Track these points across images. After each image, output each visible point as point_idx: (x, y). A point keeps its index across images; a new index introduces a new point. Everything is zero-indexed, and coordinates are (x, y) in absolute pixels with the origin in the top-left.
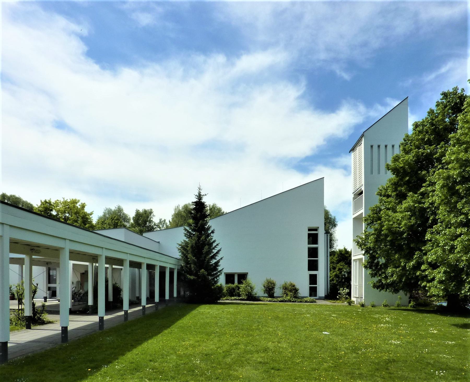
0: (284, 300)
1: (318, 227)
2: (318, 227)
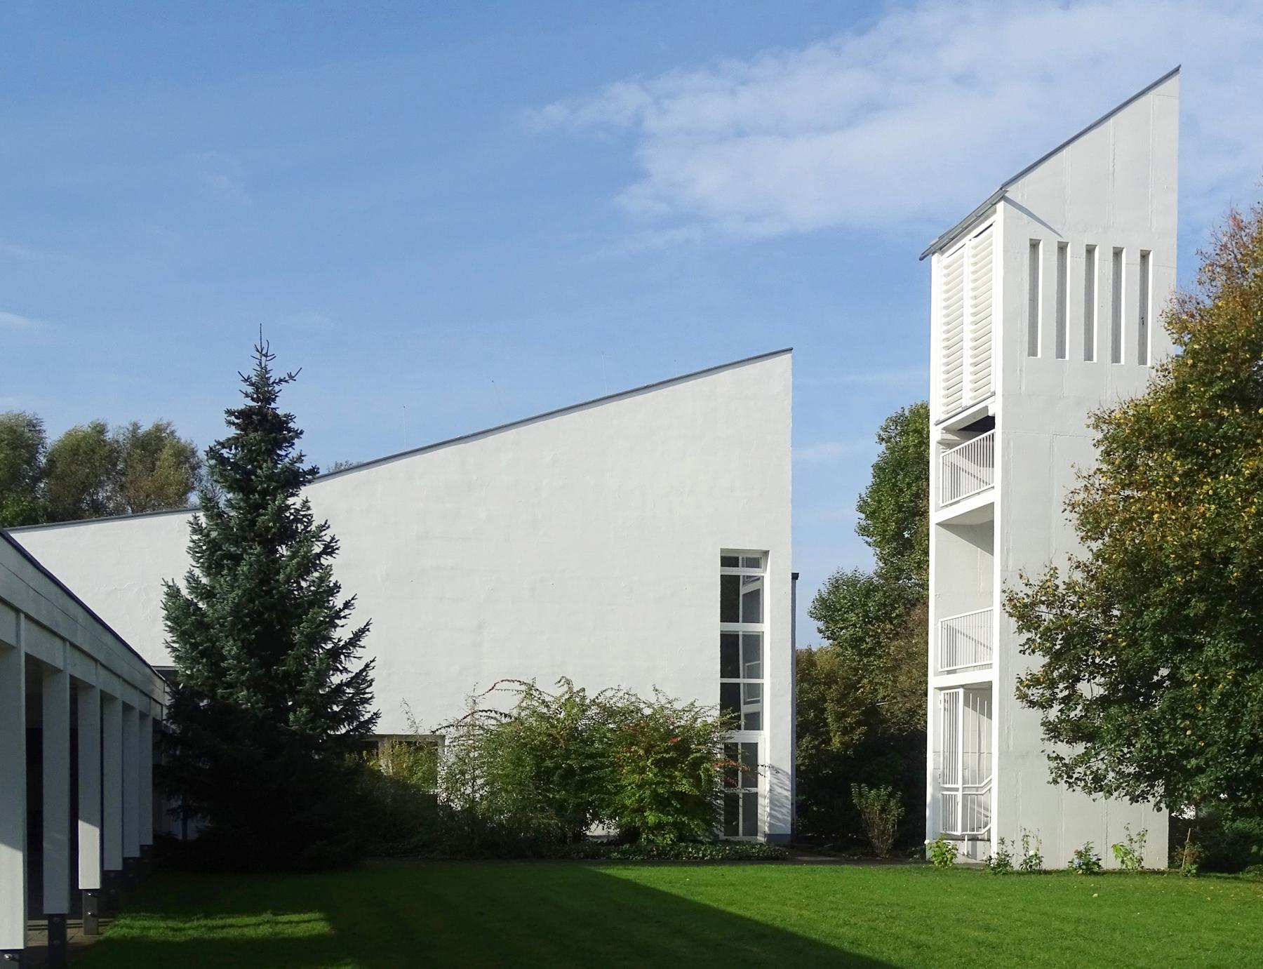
1: (766, 553)
2: (766, 553)
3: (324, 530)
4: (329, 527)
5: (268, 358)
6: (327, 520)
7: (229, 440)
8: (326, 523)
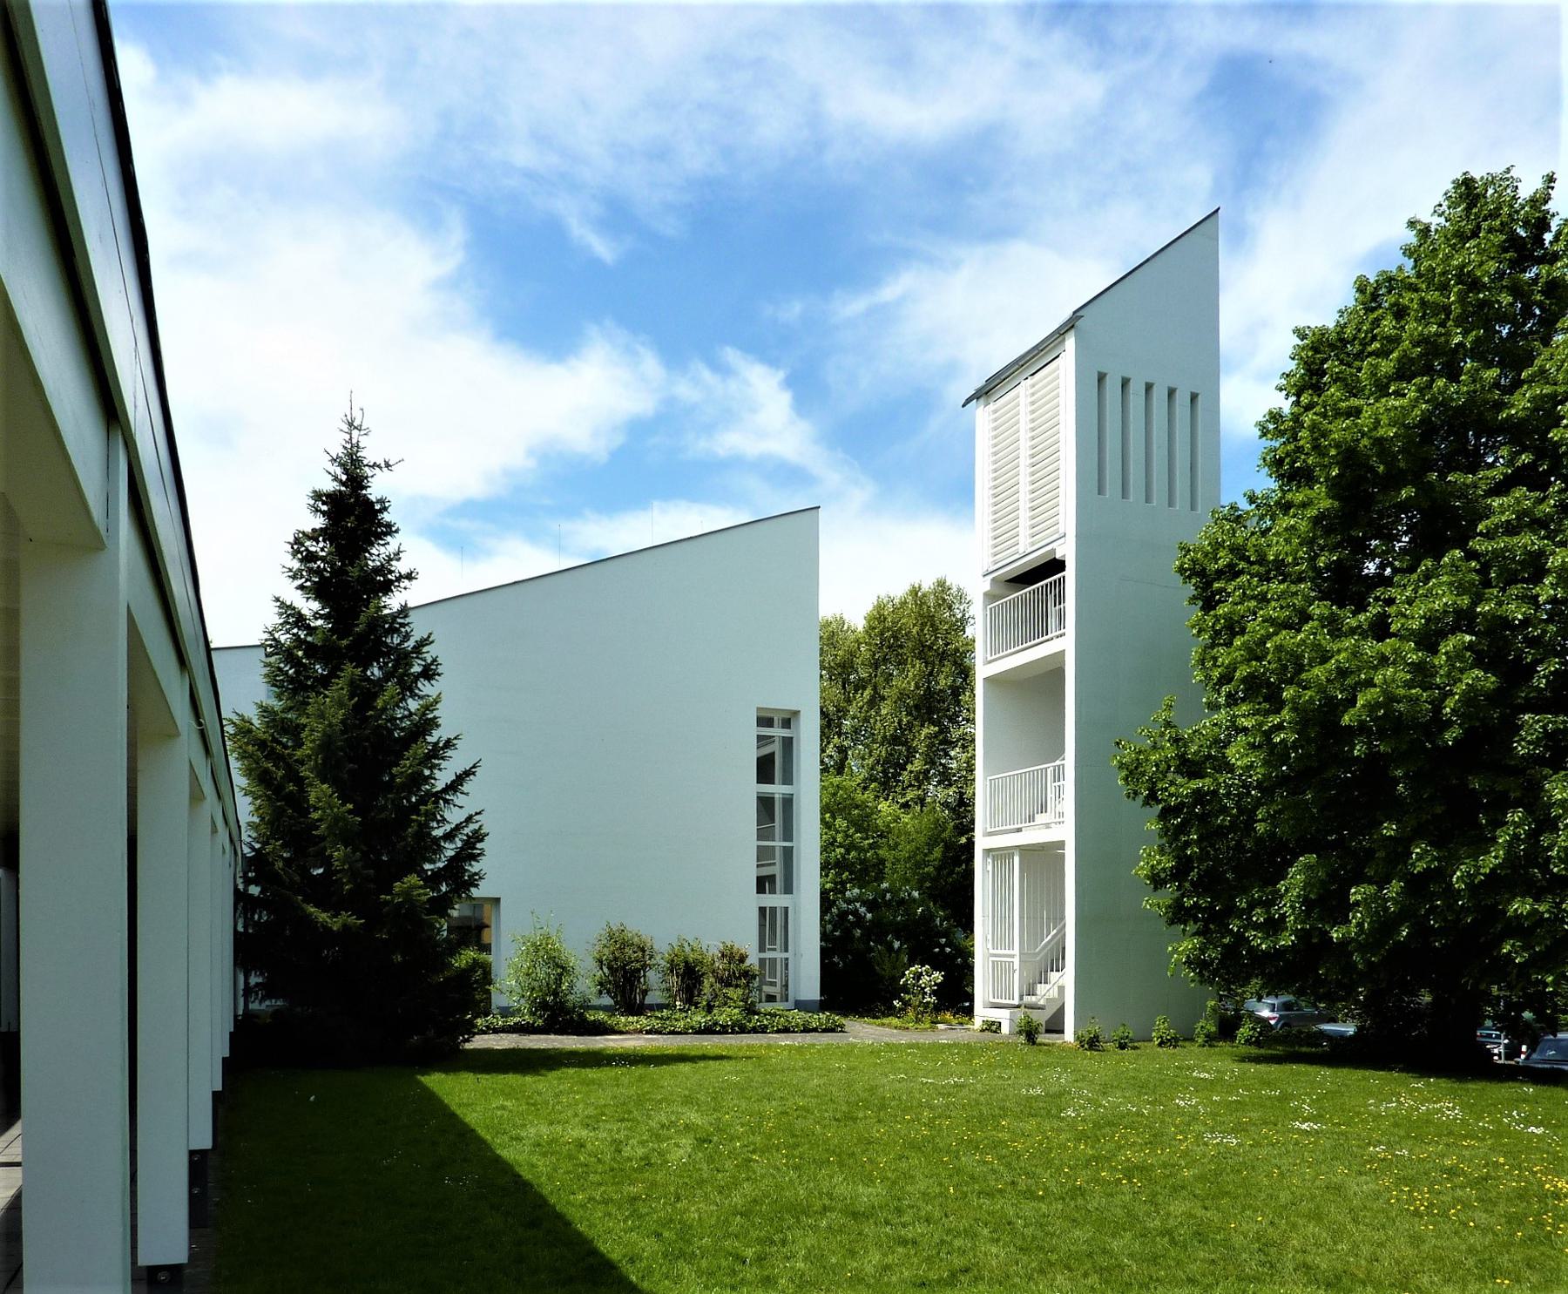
0: (716, 1024)
3: (427, 644)
4: (432, 642)
5: (362, 432)
6: (431, 634)
7: (314, 530)
8: (429, 637)
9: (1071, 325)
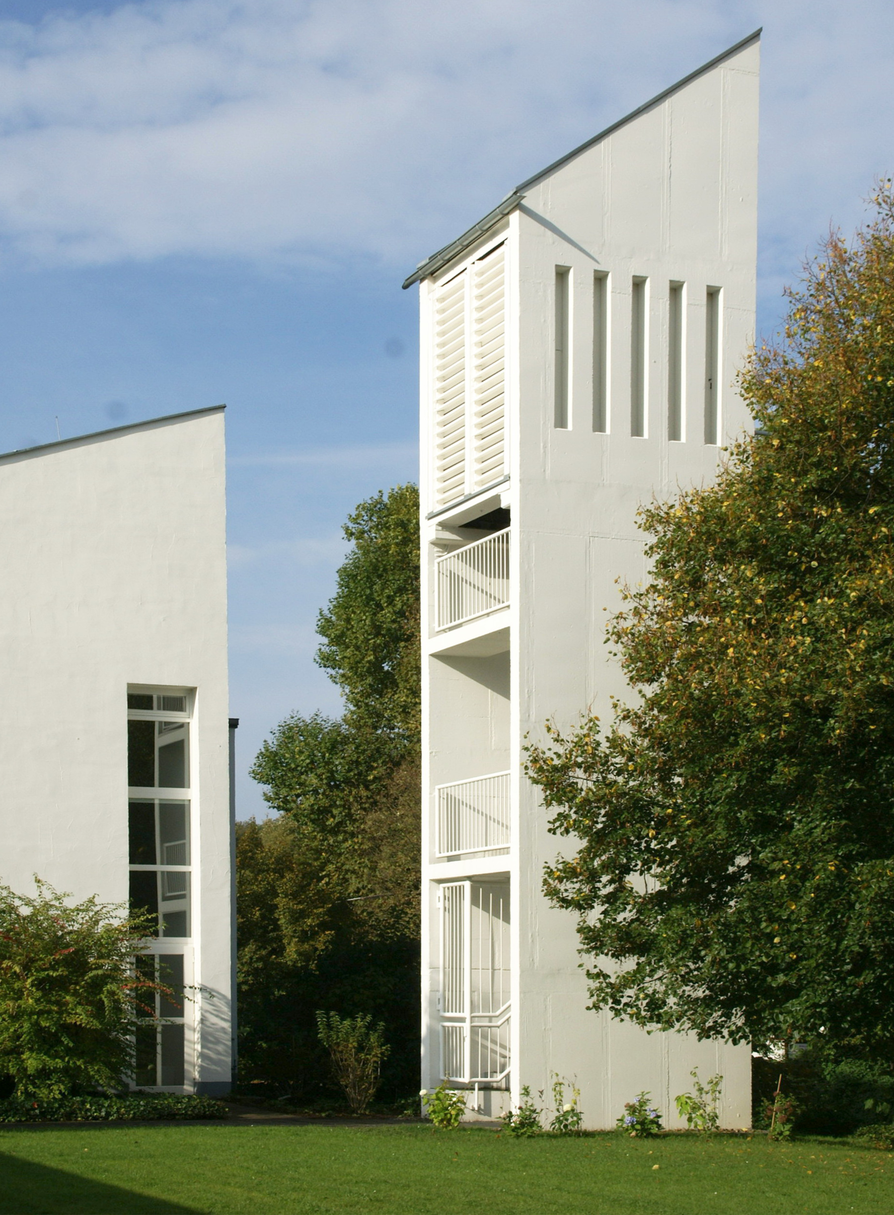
9: (515, 204)
